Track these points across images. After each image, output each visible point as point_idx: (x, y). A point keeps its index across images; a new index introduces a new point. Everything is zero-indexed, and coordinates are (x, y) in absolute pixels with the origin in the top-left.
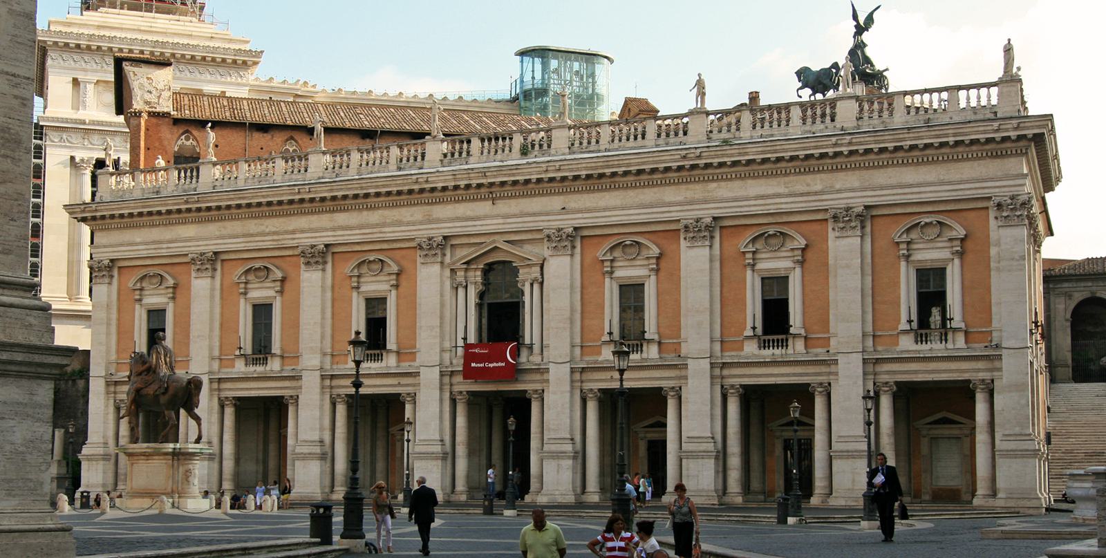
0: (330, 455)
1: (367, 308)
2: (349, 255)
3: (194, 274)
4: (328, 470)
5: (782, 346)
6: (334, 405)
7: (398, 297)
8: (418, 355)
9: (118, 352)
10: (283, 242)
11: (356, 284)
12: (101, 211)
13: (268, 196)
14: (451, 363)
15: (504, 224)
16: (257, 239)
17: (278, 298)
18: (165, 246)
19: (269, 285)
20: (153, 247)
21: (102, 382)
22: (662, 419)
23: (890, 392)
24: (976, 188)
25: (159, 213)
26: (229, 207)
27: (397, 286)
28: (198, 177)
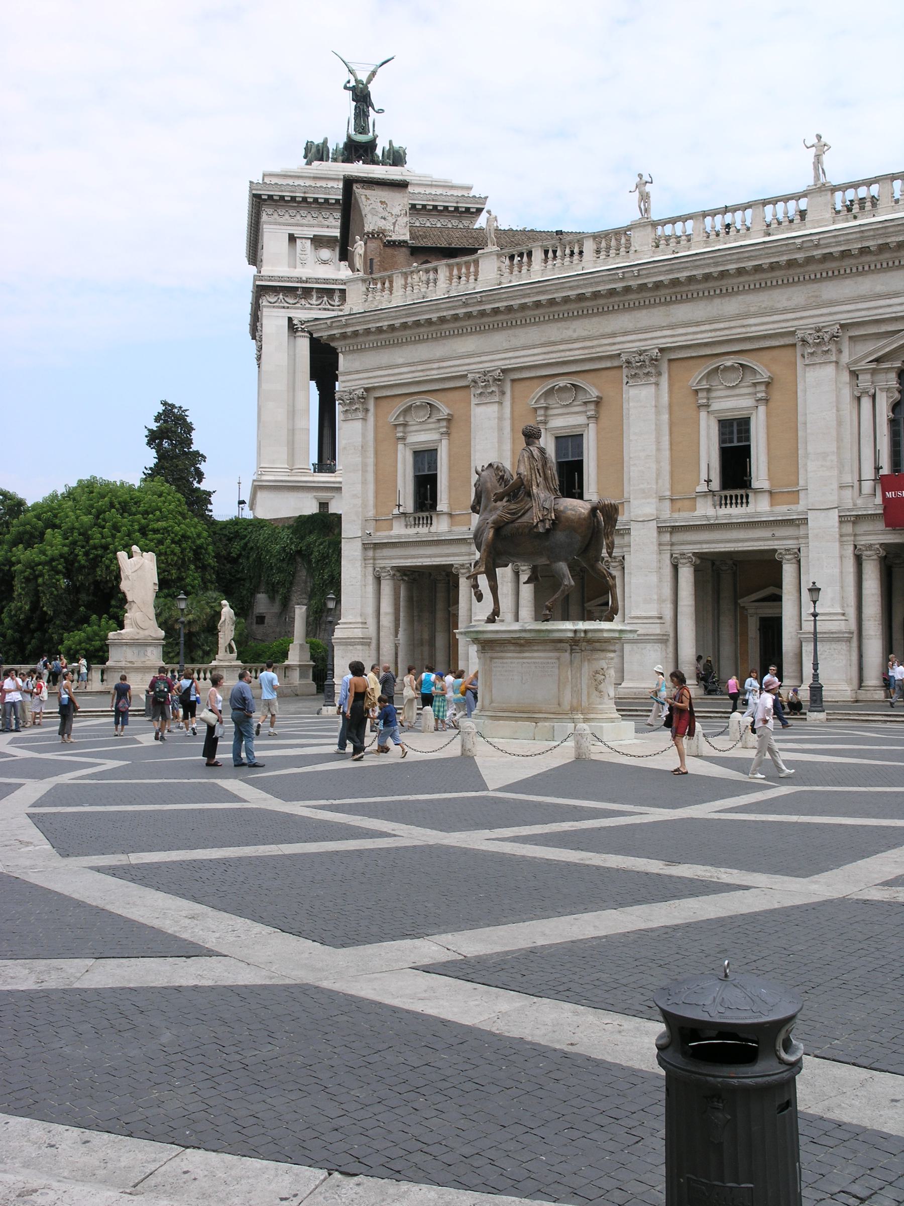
0: (672, 635)
1: (722, 433)
2: (691, 362)
3: (474, 401)
4: (671, 655)
6: (675, 568)
7: (768, 415)
8: (802, 495)
9: (376, 506)
10: (598, 350)
11: (705, 401)
12: (353, 325)
13: (578, 287)
14: (855, 505)
16: (561, 347)
17: (592, 426)
18: (436, 365)
20: (420, 368)
21: (358, 544)
23: (875, 557)
24: (868, 309)
25: (429, 322)
26: (523, 307)
28: (476, 274)
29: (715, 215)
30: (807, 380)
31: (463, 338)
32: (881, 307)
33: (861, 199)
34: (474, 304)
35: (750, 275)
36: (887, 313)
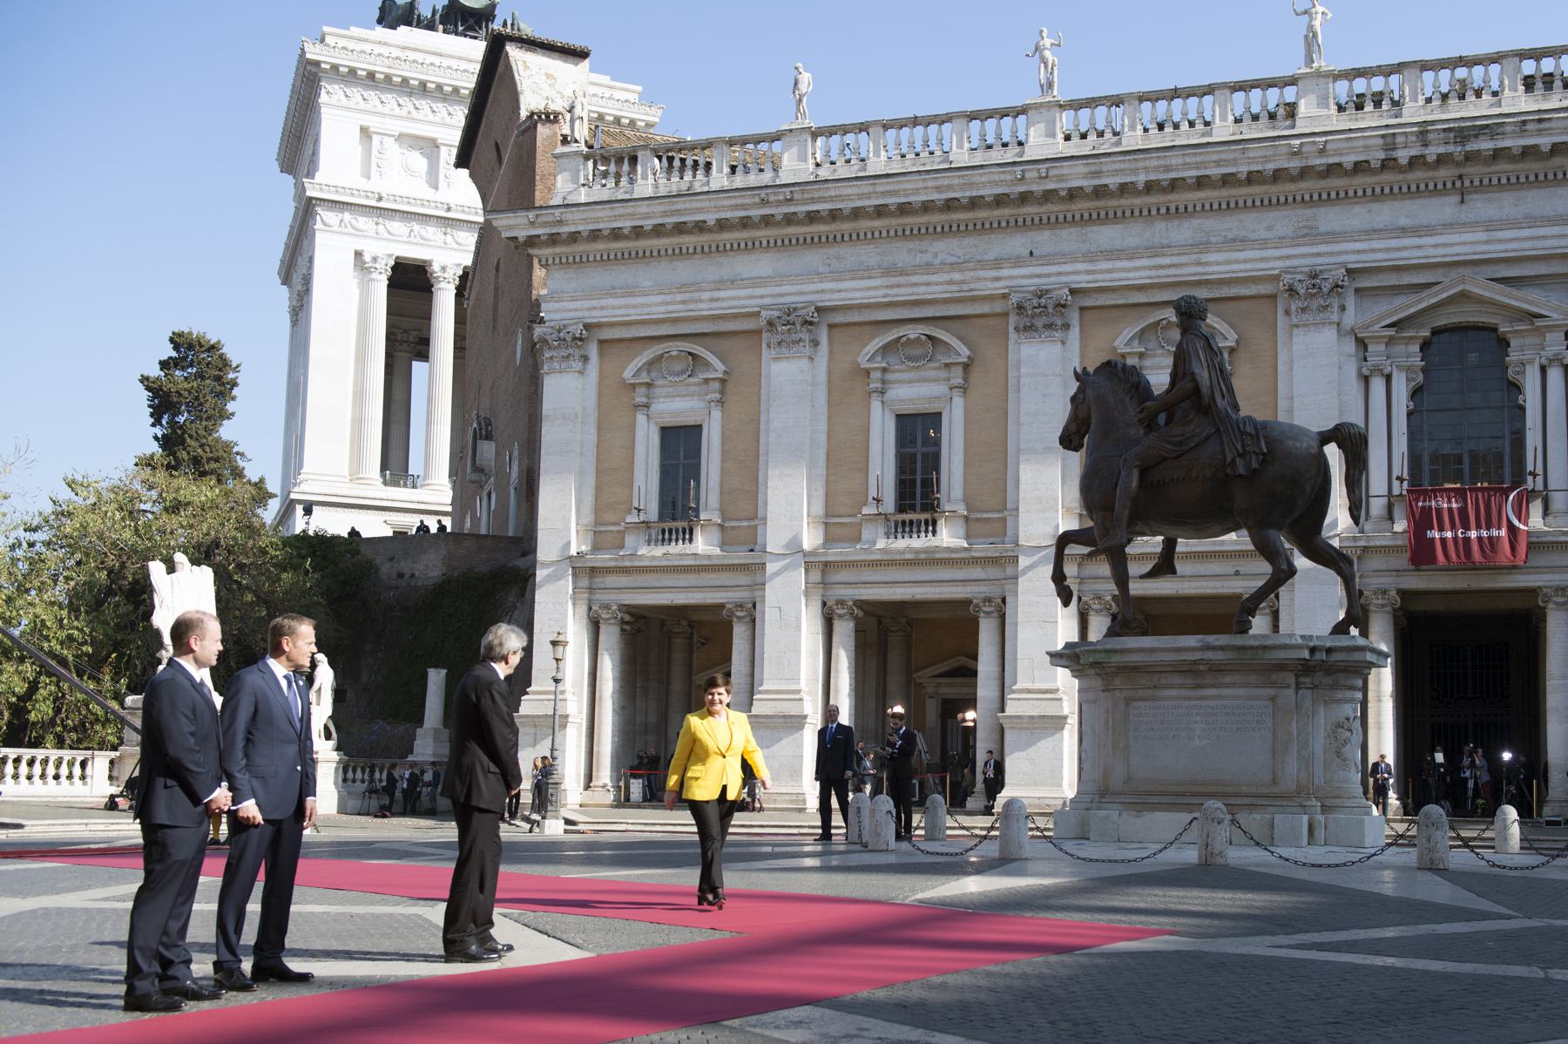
5: (926, 531)
15: (1487, 242)
17: (958, 401)
19: (932, 374)
22: (969, 662)
23: (1389, 609)
27: (964, 389)
29: (1188, 96)
30: (1295, 347)
31: (752, 257)
32: (1406, 248)
33: (1545, 75)
34: (779, 203)
35: (1401, 172)
36: (1414, 257)
